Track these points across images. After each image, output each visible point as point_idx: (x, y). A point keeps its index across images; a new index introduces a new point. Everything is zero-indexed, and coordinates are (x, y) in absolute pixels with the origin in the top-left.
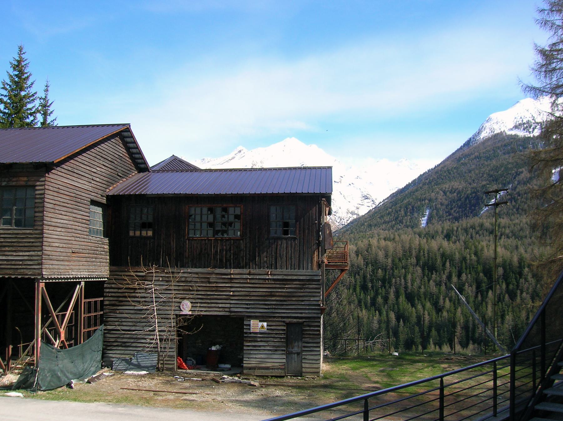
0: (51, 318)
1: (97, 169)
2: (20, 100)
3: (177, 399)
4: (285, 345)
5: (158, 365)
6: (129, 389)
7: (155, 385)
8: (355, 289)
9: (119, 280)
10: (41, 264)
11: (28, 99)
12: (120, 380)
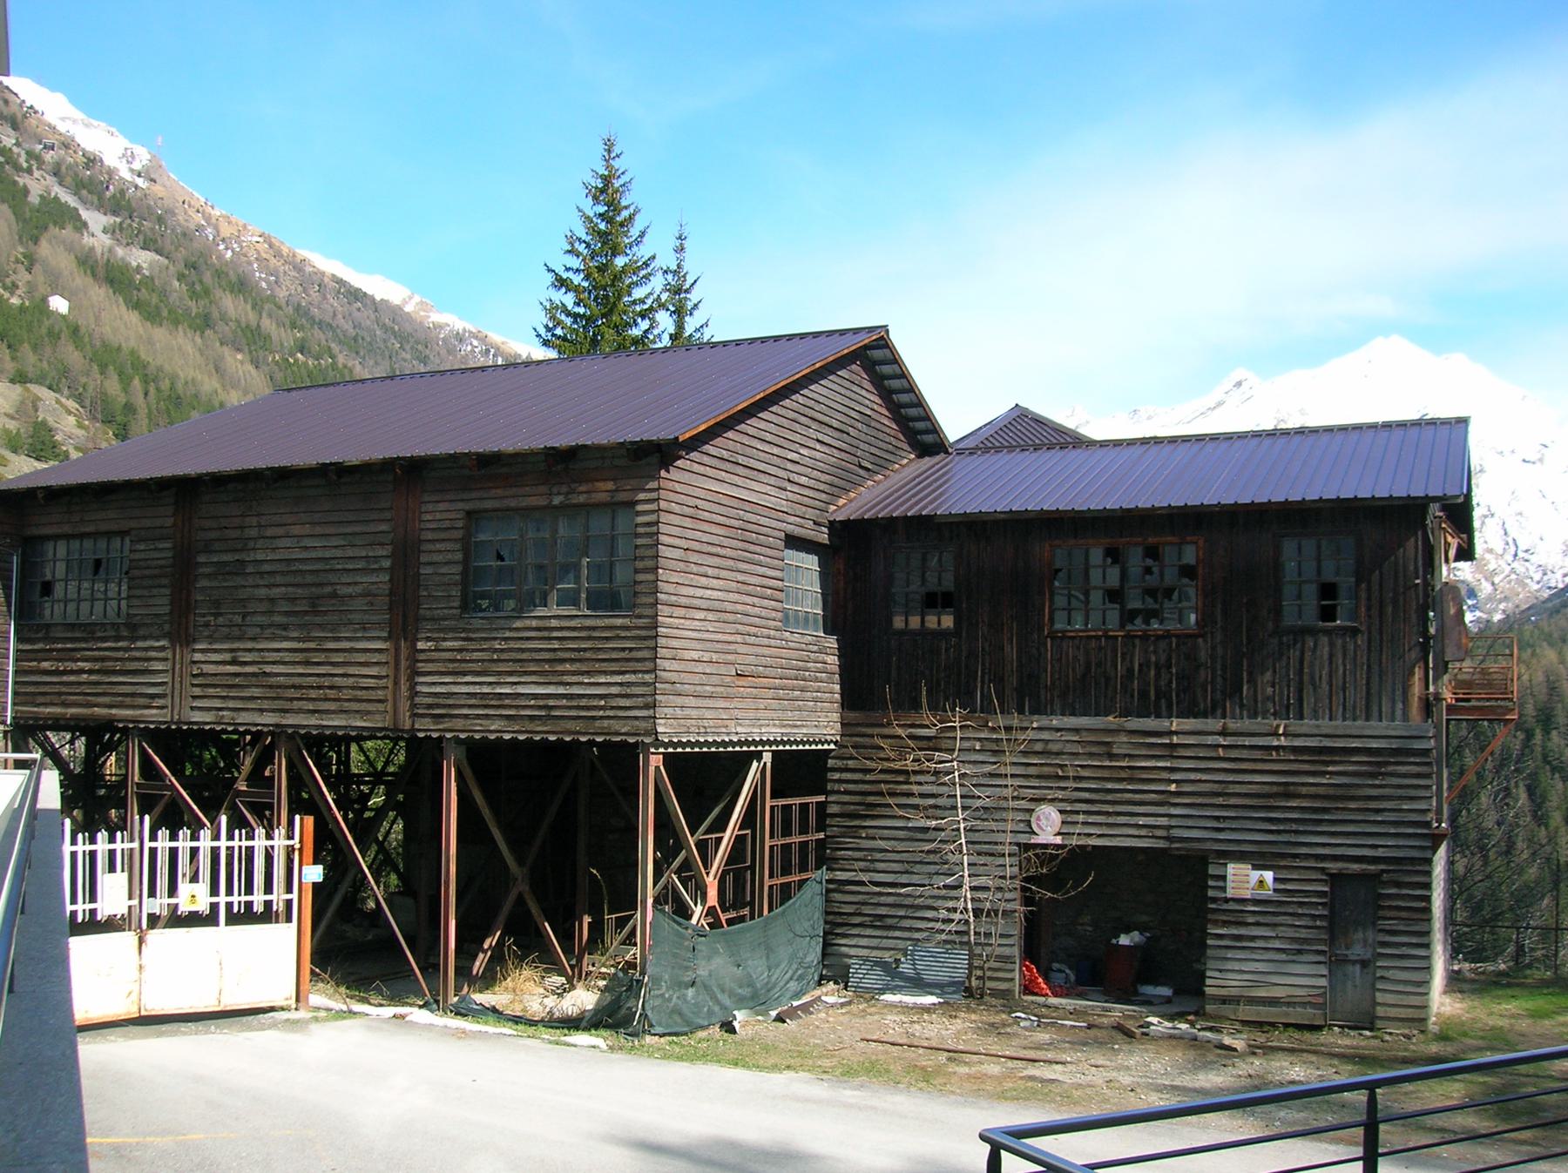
0: (684, 851)
1: (802, 451)
2: (613, 281)
3: (1009, 1075)
4: (1326, 937)
5: (970, 982)
6: (882, 1042)
7: (957, 1035)
9: (865, 747)
11: (634, 274)
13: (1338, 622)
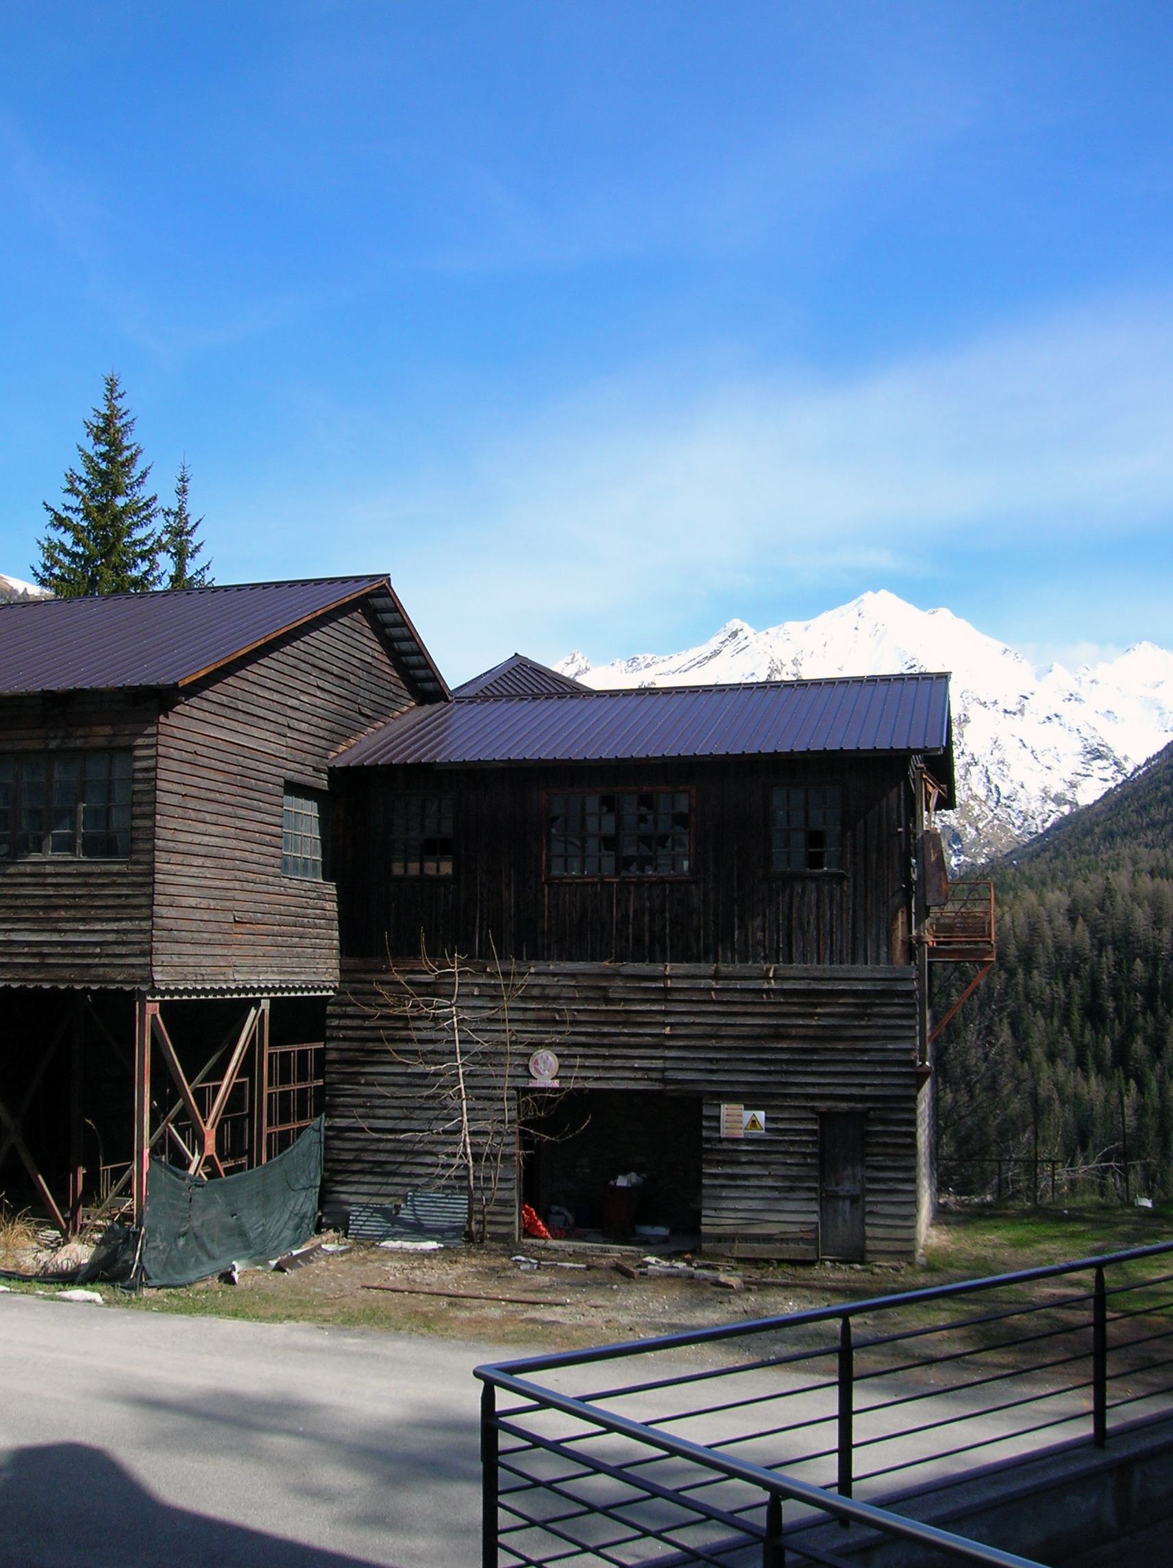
1: (302, 698)
3: (510, 1318)
4: (817, 1174)
5: (470, 1226)
6: (383, 1289)
7: (458, 1280)
8: (1066, 1019)
9: (364, 994)
10: (149, 953)
11: (135, 515)
12: (364, 1264)
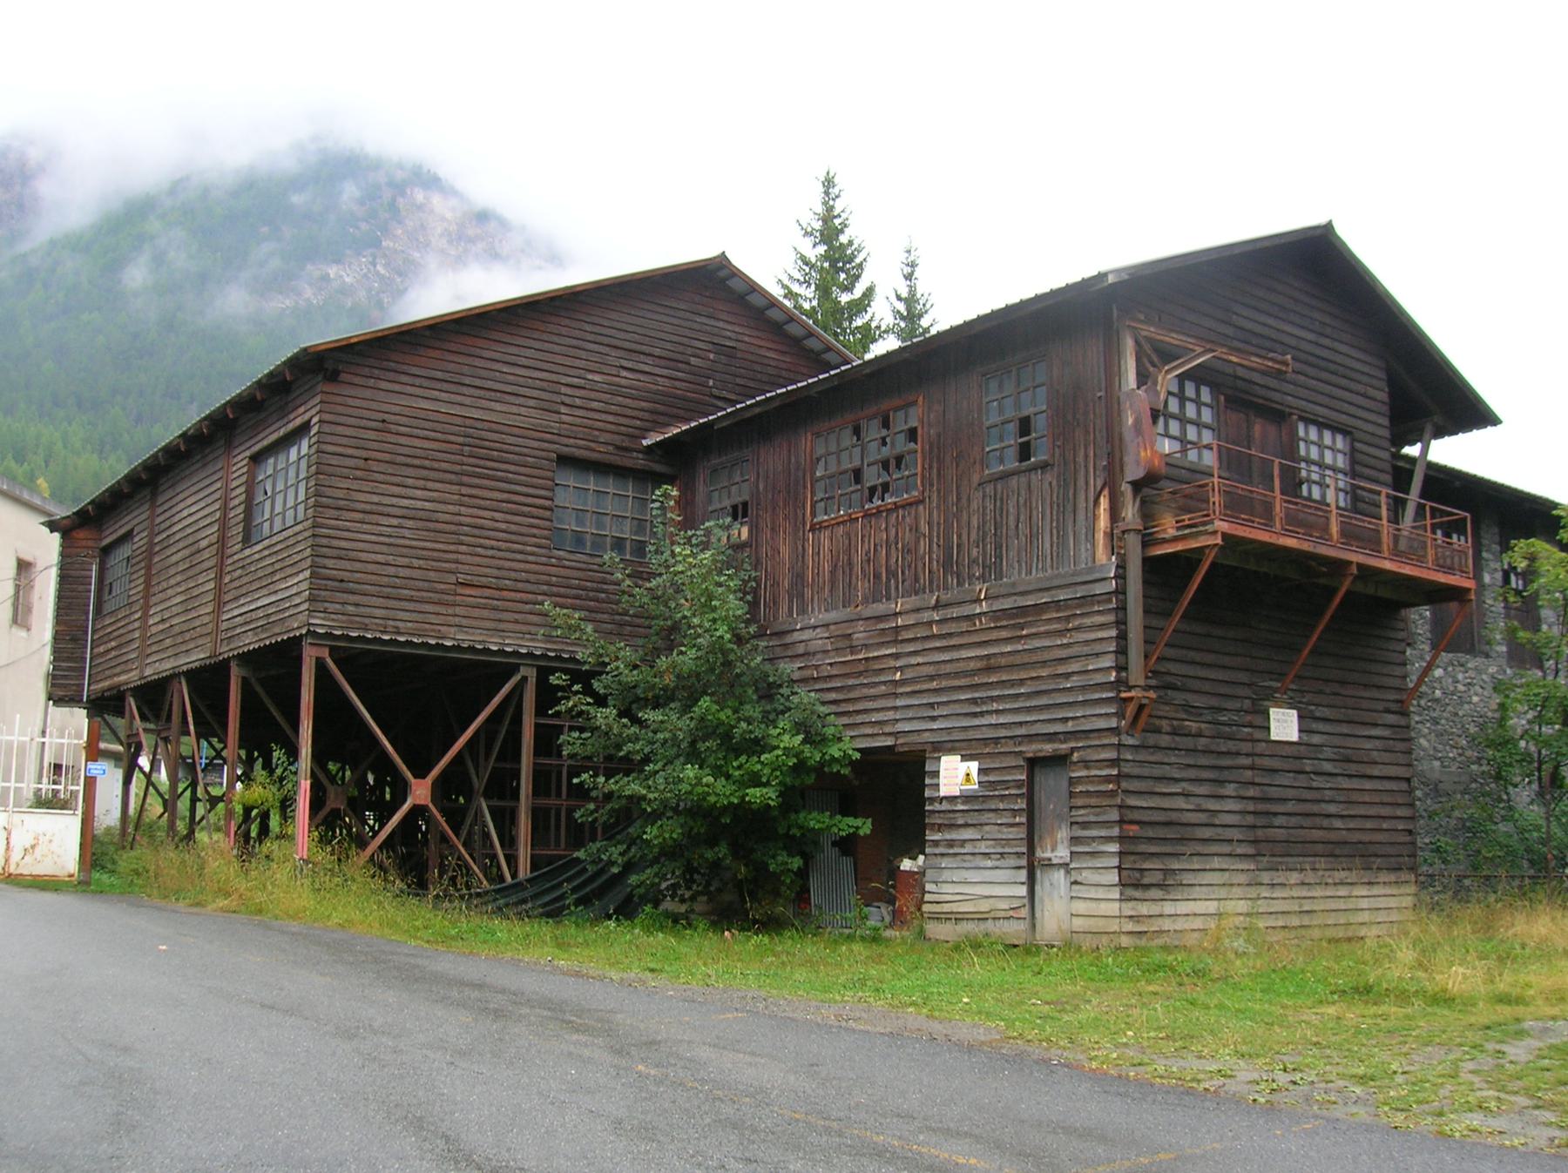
13: (1032, 459)
